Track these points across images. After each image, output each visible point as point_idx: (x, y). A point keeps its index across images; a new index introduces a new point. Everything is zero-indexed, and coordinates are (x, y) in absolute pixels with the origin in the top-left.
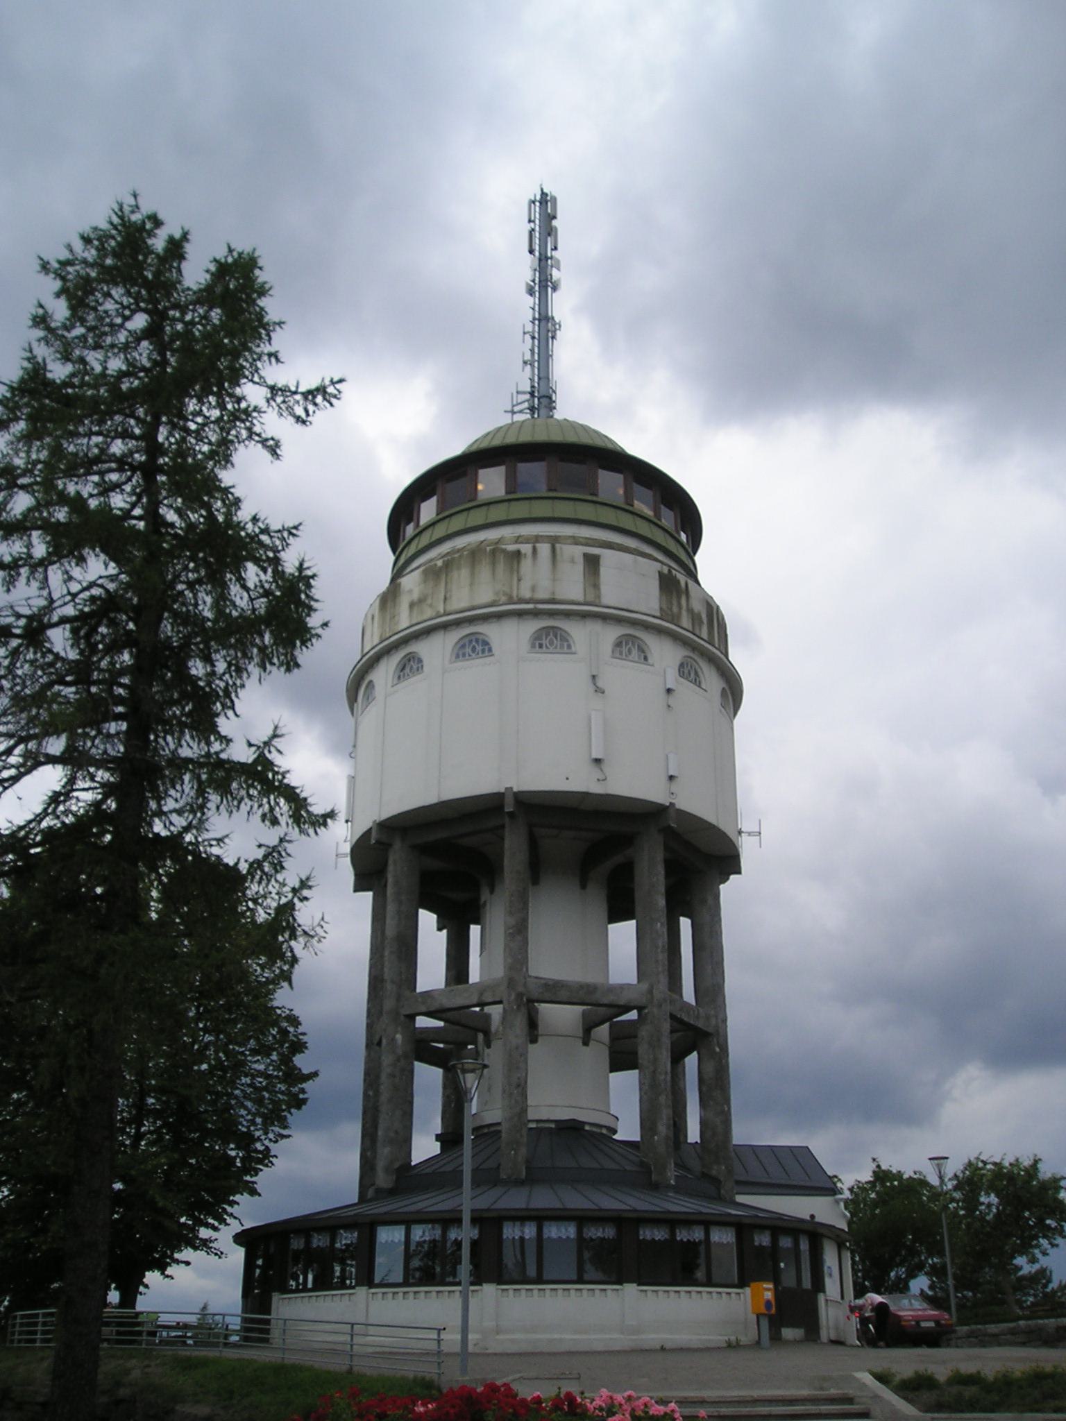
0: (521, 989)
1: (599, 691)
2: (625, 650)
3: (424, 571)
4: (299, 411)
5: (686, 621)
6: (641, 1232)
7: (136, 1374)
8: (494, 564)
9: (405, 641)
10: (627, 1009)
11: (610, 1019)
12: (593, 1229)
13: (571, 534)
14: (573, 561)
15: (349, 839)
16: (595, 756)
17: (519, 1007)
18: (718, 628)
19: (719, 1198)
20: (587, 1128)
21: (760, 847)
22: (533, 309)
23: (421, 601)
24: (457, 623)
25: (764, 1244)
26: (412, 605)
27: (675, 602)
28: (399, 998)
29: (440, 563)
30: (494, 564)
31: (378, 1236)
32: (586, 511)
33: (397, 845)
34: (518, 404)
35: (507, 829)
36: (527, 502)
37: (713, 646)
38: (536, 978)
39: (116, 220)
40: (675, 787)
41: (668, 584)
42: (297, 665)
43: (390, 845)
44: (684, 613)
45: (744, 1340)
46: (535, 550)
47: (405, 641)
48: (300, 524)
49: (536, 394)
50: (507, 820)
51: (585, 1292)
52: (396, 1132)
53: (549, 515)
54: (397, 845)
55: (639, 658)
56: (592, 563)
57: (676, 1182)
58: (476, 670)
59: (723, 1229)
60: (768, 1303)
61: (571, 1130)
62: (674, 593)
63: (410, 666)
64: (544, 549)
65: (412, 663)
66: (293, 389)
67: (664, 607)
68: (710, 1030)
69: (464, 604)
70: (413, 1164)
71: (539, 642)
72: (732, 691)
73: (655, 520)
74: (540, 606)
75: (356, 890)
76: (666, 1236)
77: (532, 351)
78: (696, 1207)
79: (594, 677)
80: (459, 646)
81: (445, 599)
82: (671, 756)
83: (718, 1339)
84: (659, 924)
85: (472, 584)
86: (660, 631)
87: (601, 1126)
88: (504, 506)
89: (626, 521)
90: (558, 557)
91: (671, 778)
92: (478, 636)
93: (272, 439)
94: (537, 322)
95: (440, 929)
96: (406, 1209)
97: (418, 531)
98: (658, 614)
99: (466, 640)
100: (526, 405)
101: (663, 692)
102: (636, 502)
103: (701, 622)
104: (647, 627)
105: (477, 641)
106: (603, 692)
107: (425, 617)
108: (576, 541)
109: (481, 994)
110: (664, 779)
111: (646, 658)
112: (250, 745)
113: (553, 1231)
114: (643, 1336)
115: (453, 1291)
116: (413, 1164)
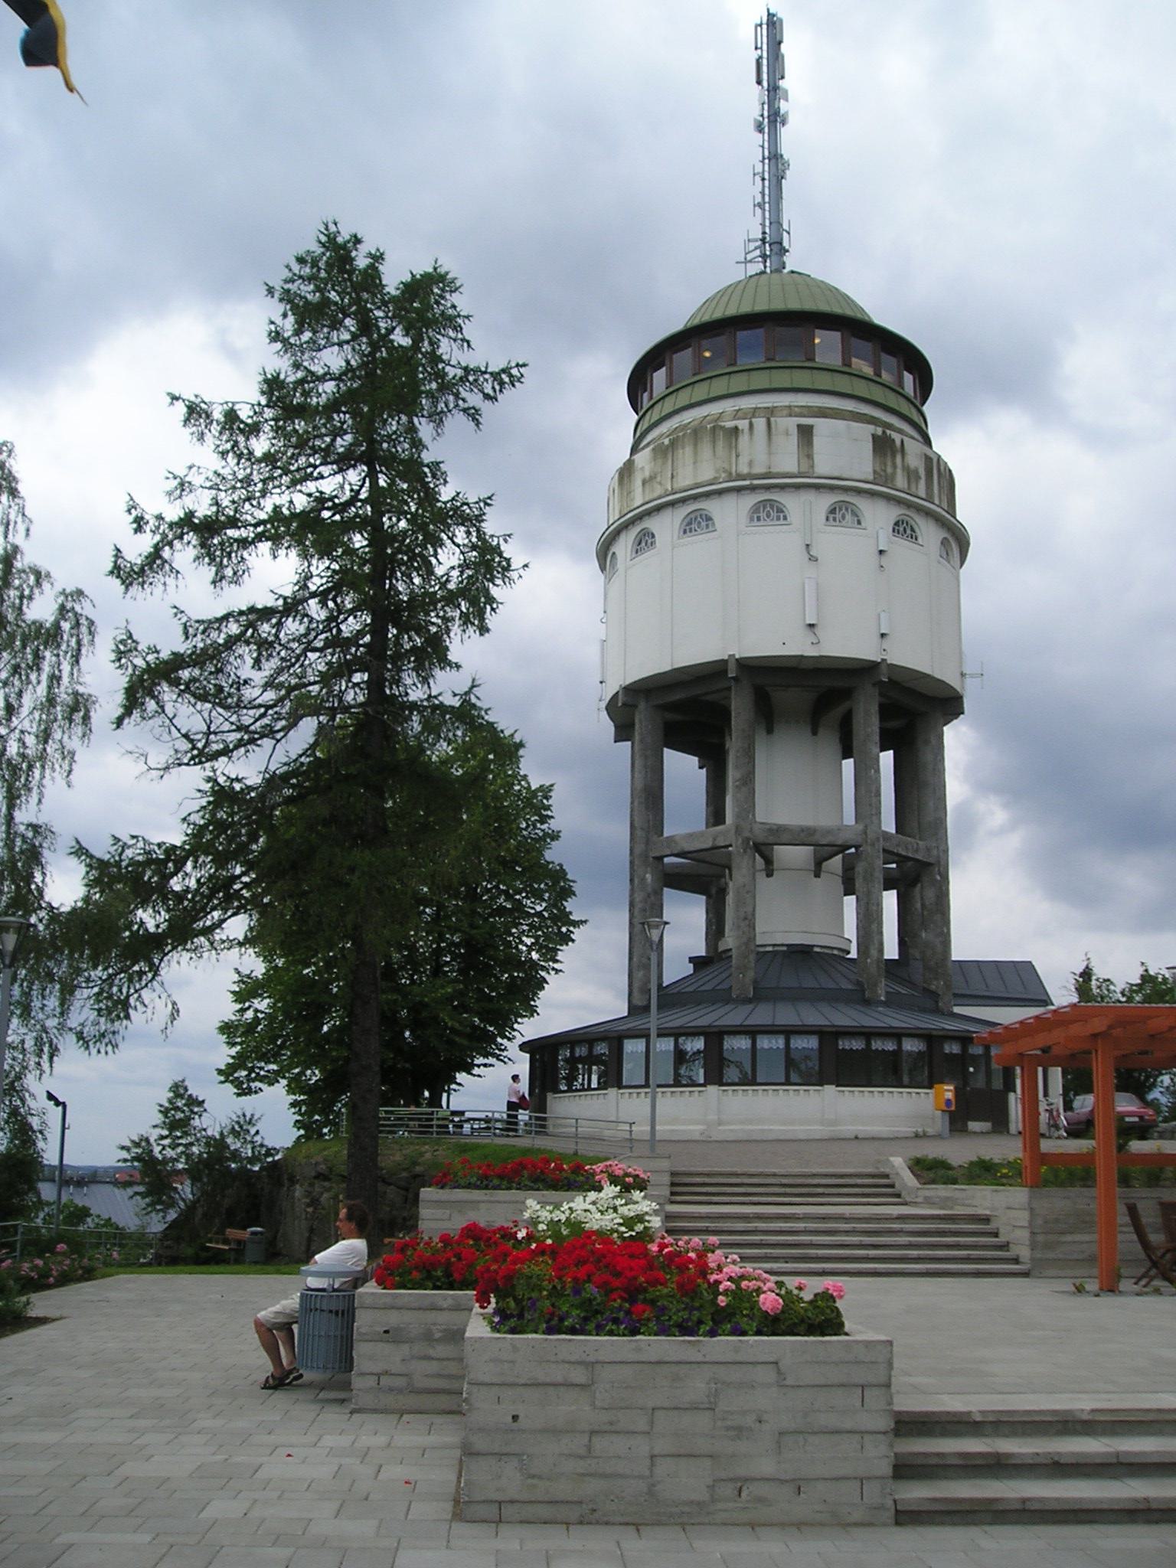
0: (747, 834)
1: (813, 559)
2: (838, 516)
3: (653, 449)
4: (489, 390)
5: (901, 481)
6: (840, 1043)
7: (428, 1156)
8: (714, 442)
9: (640, 517)
10: (850, 847)
11: (842, 852)
12: (799, 1042)
13: (787, 404)
14: (787, 434)
17: (745, 851)
19: (937, 1011)
22: (763, 147)
23: (652, 478)
24: (683, 501)
25: (955, 1052)
26: (644, 482)
27: (889, 463)
28: (647, 842)
29: (666, 441)
30: (714, 442)
31: (625, 1046)
32: (802, 378)
33: (642, 705)
36: (746, 374)
37: (933, 503)
39: (324, 239)
40: (886, 644)
42: (488, 630)
43: (635, 706)
44: (899, 471)
45: (930, 1131)
46: (751, 425)
47: (640, 517)
49: (768, 239)
50: (733, 683)
51: (791, 1093)
53: (767, 386)
54: (642, 705)
55: (853, 523)
56: (806, 433)
57: (886, 997)
58: (700, 545)
60: (948, 1102)
61: (801, 954)
62: (889, 454)
63: (645, 541)
64: (760, 423)
66: (483, 369)
67: (878, 469)
68: (931, 860)
69: (688, 482)
71: (758, 513)
72: (957, 541)
73: (874, 378)
76: (863, 1046)
77: (763, 194)
81: (672, 477)
82: (883, 615)
83: (906, 1130)
85: (695, 463)
89: (843, 384)
90: (773, 430)
91: (883, 635)
93: (474, 408)
94: (767, 161)
95: (701, 767)
96: (666, 1025)
97: (651, 403)
98: (871, 478)
100: (758, 252)
101: (877, 553)
102: (854, 360)
103: (918, 478)
104: (859, 492)
106: (817, 560)
107: (656, 495)
108: (791, 411)
109: (715, 839)
110: (876, 638)
111: (859, 522)
112: (455, 695)
113: (764, 1042)
114: (839, 1128)
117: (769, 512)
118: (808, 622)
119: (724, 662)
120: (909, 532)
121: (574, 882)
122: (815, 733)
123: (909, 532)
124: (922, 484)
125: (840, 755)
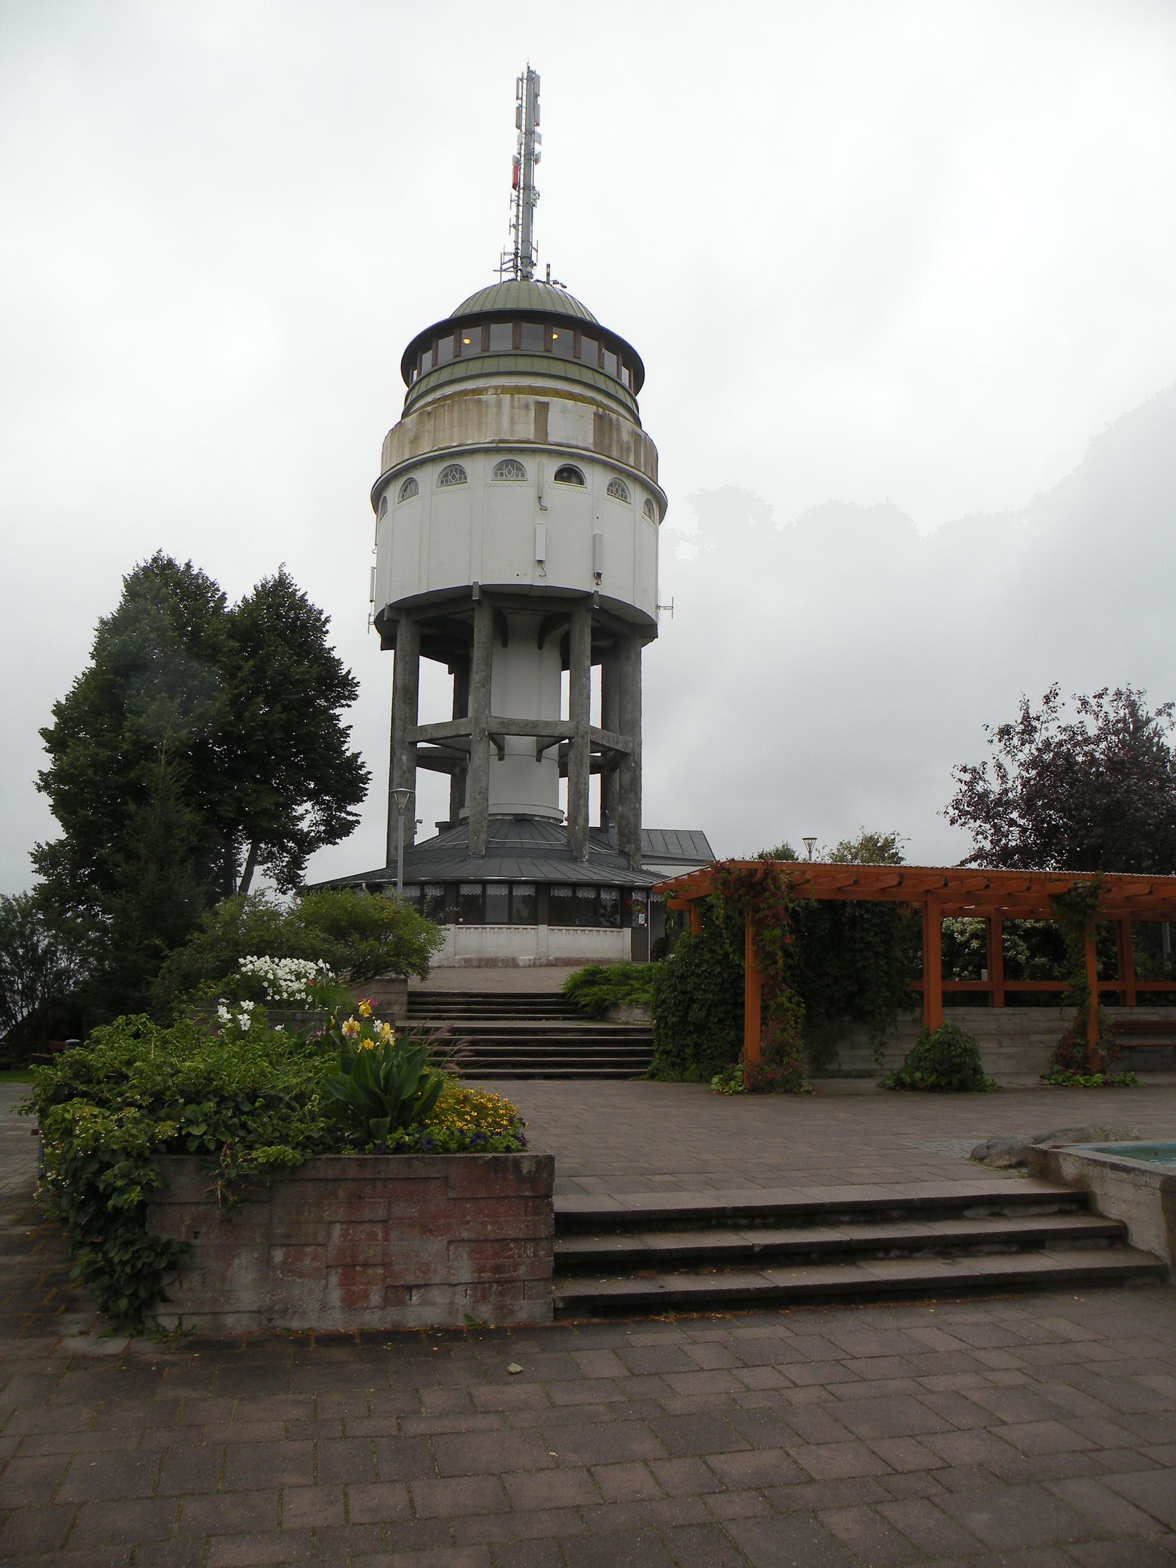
1: (544, 509)
15: (373, 613)
18: (646, 454)
20: (536, 819)
24: (442, 457)
33: (403, 621)
34: (504, 263)
35: (476, 612)
38: (495, 717)
41: (603, 423)
44: (614, 444)
54: (403, 621)
59: (525, 886)
61: (522, 820)
68: (628, 751)
70: (415, 844)
72: (657, 503)
74: (500, 445)
75: (382, 650)
77: (517, 216)
78: (609, 875)
80: (442, 475)
86: (593, 460)
88: (479, 362)
99: (448, 470)
100: (511, 264)
105: (456, 471)
116: (415, 844)
117: (454, 476)
119: (469, 588)
120: (620, 492)
122: (540, 647)
123: (620, 492)
124: (632, 455)
125: (558, 662)
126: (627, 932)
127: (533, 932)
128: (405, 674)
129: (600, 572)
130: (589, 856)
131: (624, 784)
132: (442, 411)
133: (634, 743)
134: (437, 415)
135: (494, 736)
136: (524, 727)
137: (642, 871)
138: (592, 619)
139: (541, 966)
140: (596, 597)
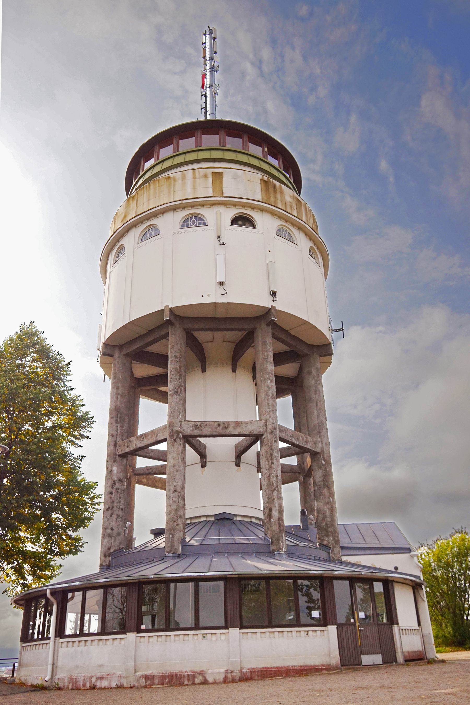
16: (219, 280)
21: (342, 322)
48: (94, 417)
51: (276, 634)
52: (112, 529)
65: (150, 231)
68: (317, 450)
79: (219, 237)
80: (184, 219)
84: (269, 381)
86: (262, 210)
87: (251, 517)
92: (196, 215)
115: (109, 639)
118: (219, 281)
121: (349, 605)
126: (332, 629)
127: (223, 637)
128: (117, 398)
129: (275, 290)
130: (287, 549)
131: (317, 481)
132: (142, 192)
133: (322, 443)
134: (139, 196)
135: (190, 439)
136: (216, 428)
137: (342, 563)
138: (272, 337)
139: (234, 681)
140: (272, 310)
